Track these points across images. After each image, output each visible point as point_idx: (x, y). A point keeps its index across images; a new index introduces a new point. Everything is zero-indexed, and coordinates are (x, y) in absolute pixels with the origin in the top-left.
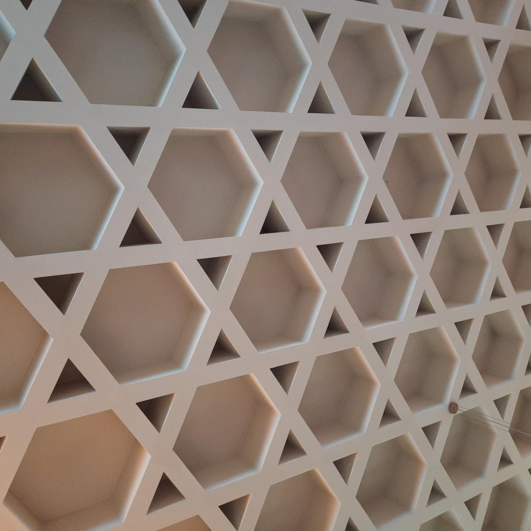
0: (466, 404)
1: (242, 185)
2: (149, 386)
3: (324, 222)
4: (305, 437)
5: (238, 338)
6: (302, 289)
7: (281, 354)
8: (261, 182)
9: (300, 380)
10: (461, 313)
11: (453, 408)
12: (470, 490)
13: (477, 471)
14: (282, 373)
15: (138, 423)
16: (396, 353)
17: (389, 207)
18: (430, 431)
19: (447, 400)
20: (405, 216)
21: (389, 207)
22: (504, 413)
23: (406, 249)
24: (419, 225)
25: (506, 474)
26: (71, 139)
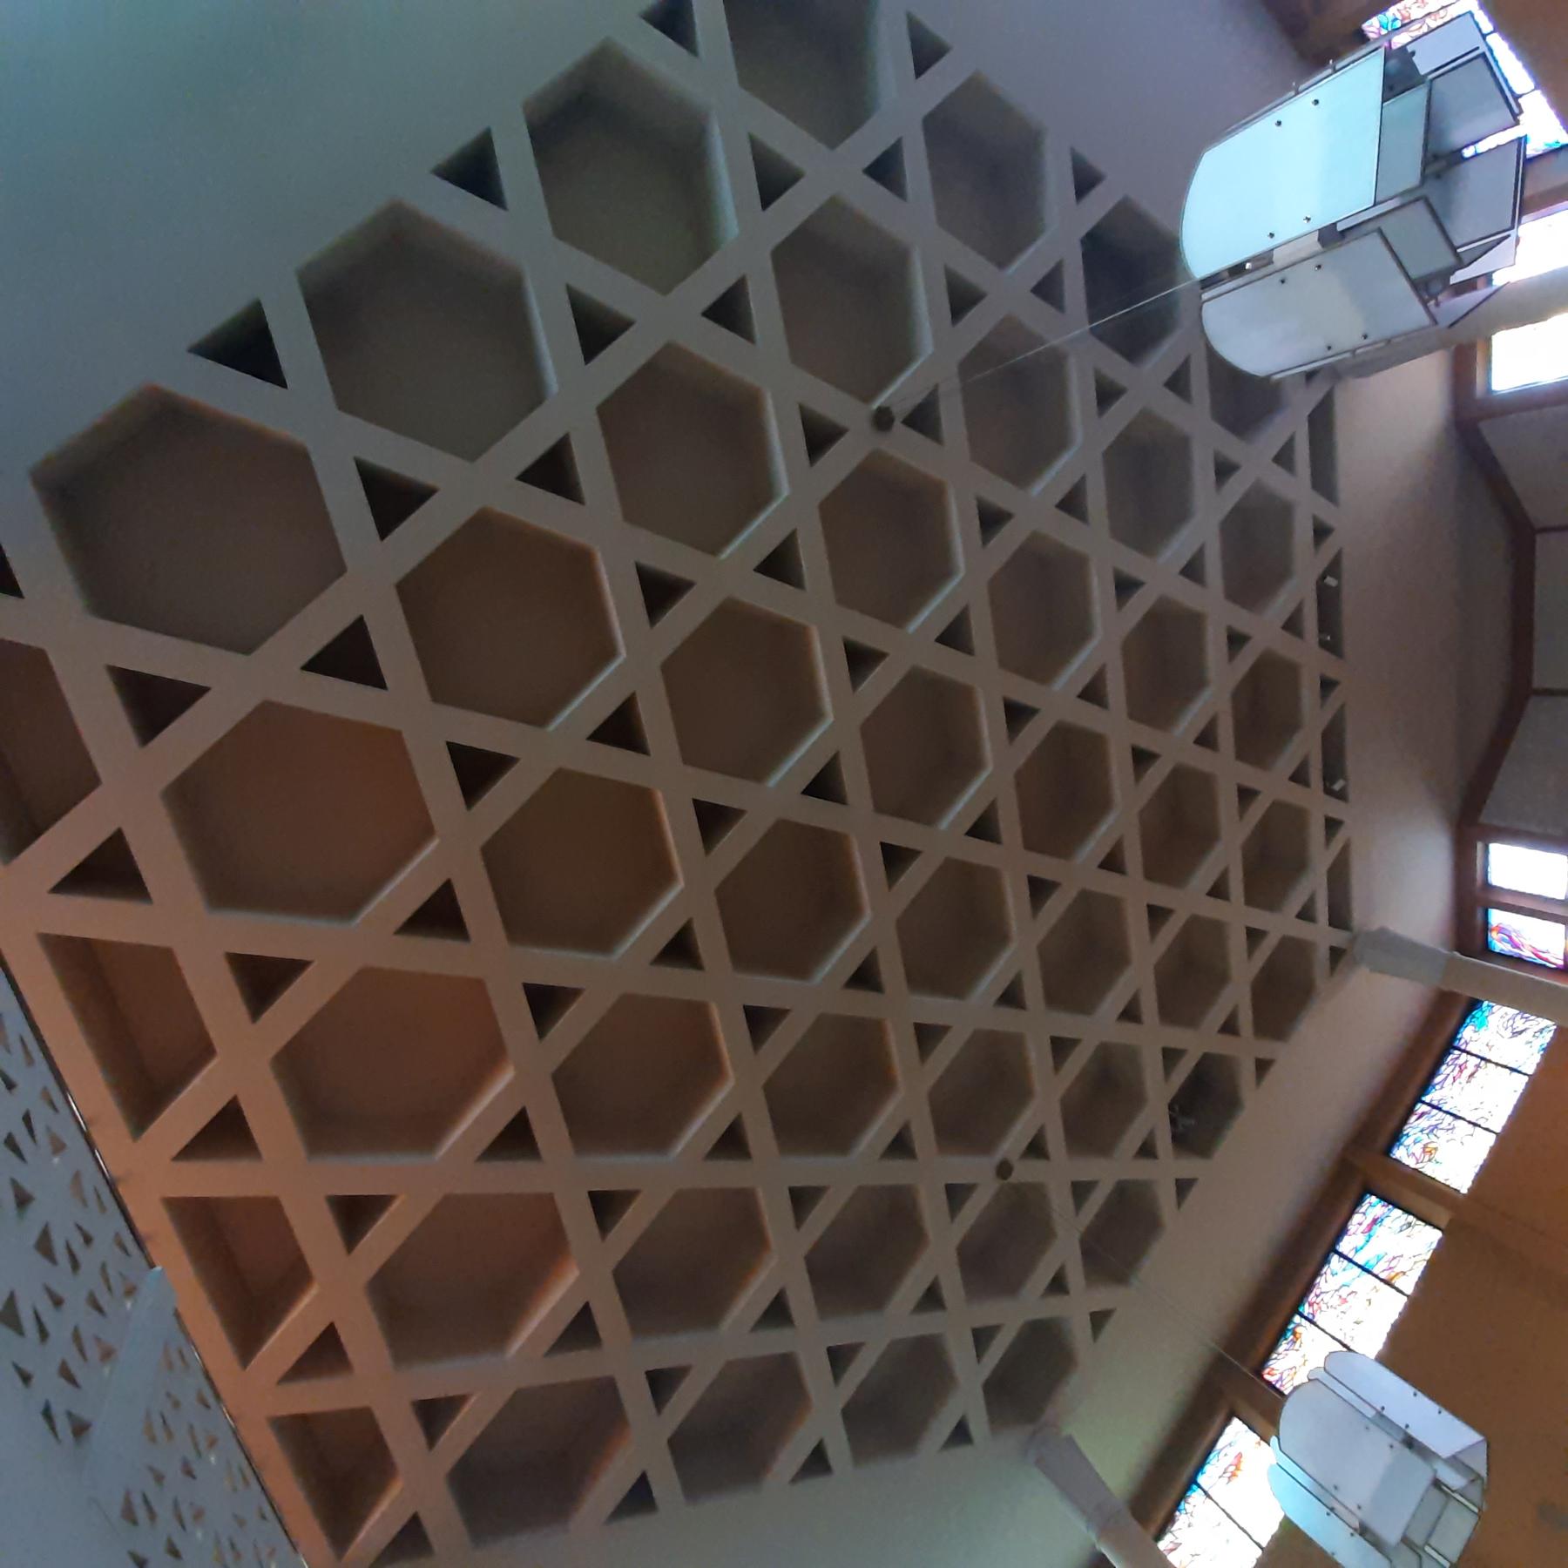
0: (1026, 1172)
1: (801, 712)
2: (553, 965)
3: (901, 812)
4: (760, 1133)
5: (711, 941)
6: (836, 905)
7: (767, 989)
8: (829, 719)
9: (783, 1039)
10: (1066, 1024)
11: (1004, 1170)
12: (989, 1312)
13: (1010, 1286)
14: (760, 1021)
15: (514, 1016)
16: (946, 1053)
17: (1009, 823)
18: (956, 1195)
19: (998, 1156)
20: (1029, 845)
21: (1009, 823)
22: (844, 1370)
23: (1015, 897)
24: (1046, 867)
25: (1052, 1308)
26: (578, 562)
